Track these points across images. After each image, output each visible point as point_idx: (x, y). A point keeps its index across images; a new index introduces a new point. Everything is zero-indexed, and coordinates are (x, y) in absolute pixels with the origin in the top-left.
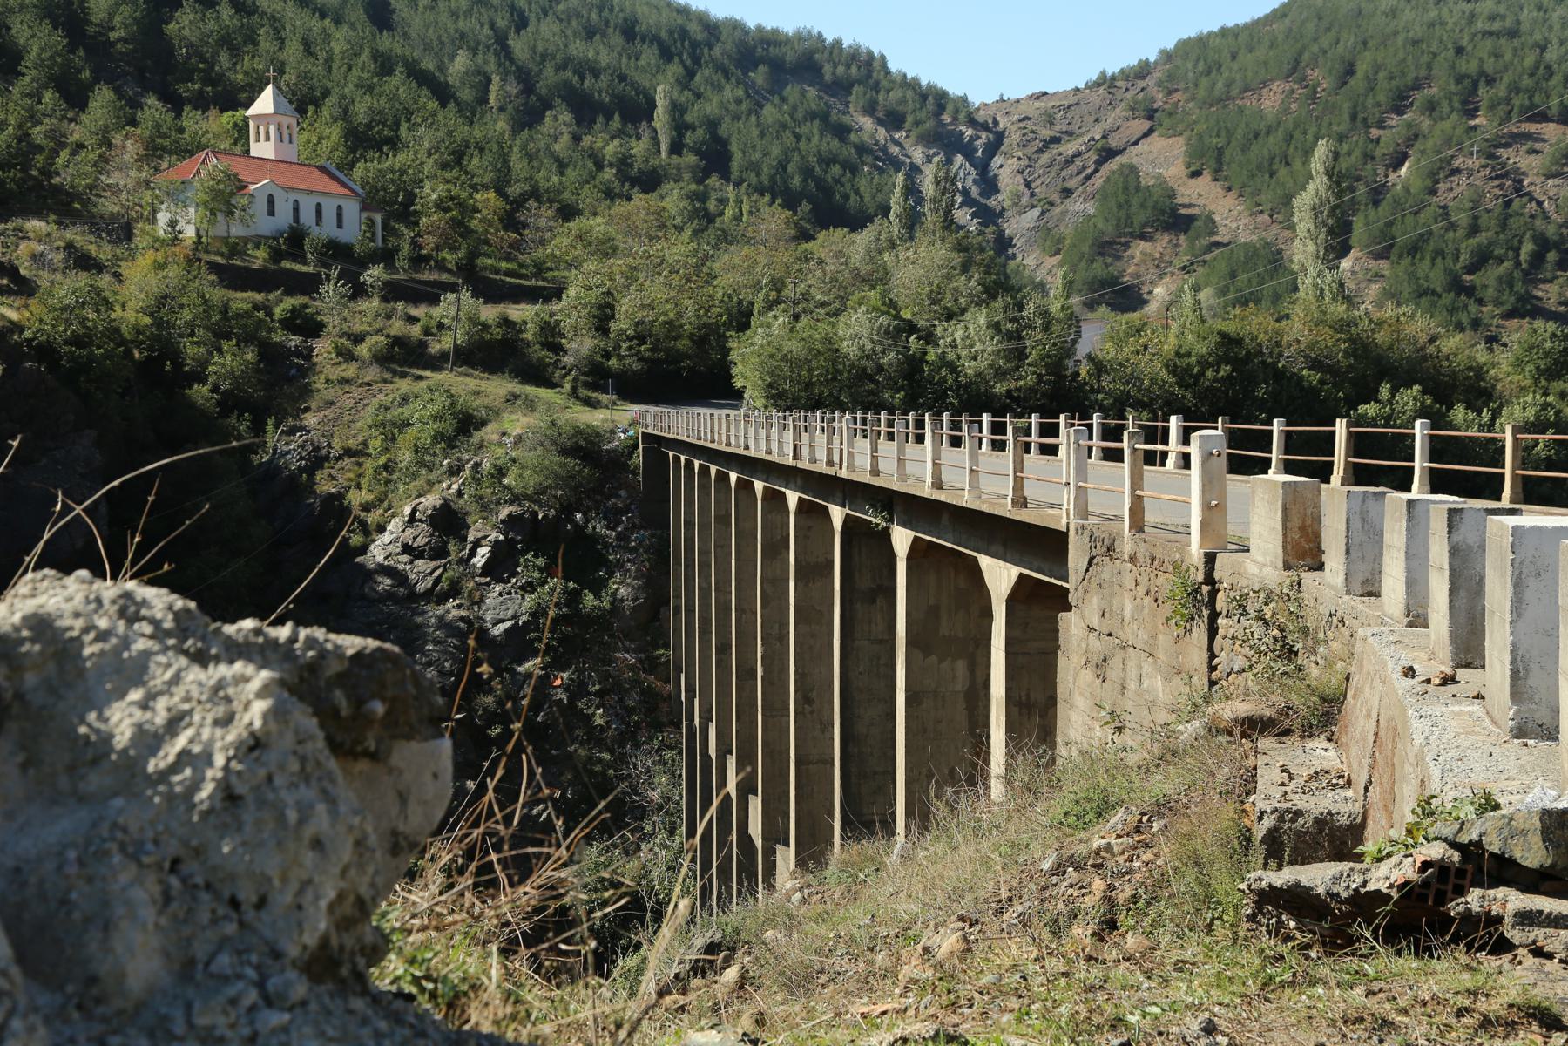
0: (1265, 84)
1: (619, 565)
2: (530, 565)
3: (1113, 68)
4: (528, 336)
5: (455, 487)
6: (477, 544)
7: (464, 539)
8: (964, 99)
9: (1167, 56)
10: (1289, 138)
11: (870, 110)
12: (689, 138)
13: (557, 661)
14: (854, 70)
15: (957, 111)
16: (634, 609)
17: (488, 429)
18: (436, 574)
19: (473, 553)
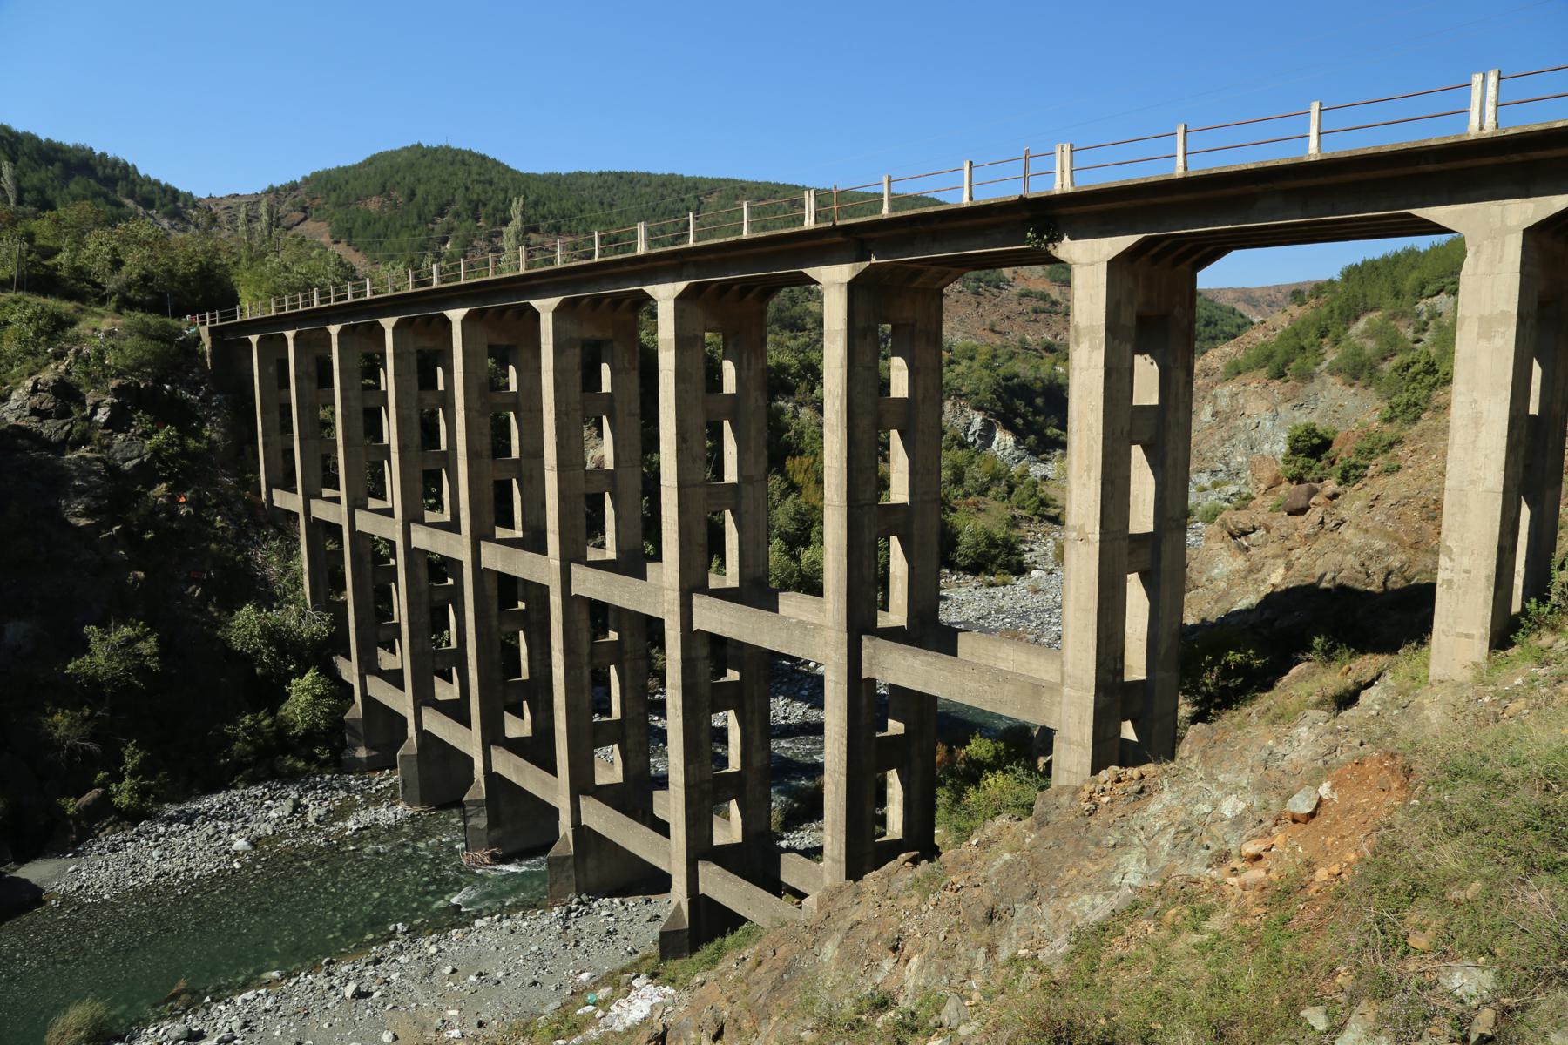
0: (367, 197)
1: (207, 418)
2: (141, 421)
3: (277, 184)
4: (64, 273)
5: (62, 367)
6: (96, 406)
7: (83, 404)
8: (190, 194)
9: (306, 180)
10: (387, 226)
11: (131, 195)
12: (27, 197)
13: (177, 487)
14: (117, 171)
15: (186, 201)
16: (225, 448)
17: (82, 325)
18: (67, 428)
19: (94, 412)
